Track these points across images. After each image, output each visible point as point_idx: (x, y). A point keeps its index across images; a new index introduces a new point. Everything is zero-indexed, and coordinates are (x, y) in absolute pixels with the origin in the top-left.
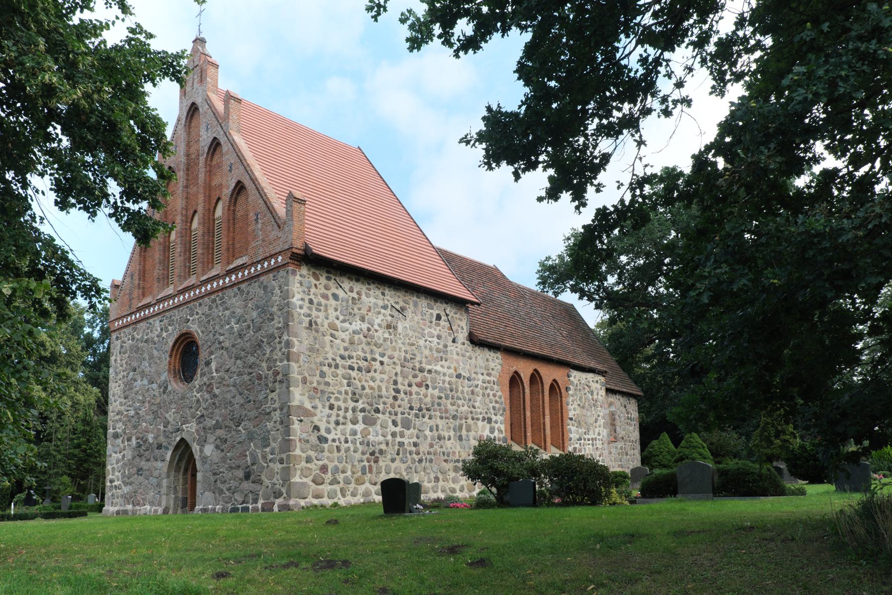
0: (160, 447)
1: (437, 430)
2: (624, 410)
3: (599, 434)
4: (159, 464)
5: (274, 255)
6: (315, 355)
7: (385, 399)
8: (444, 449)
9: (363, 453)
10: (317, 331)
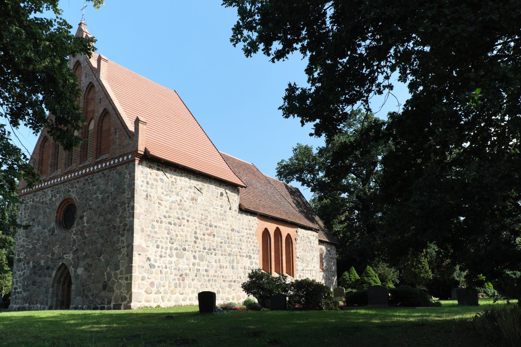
0: (48, 268)
4: (47, 279)
9: (176, 275)
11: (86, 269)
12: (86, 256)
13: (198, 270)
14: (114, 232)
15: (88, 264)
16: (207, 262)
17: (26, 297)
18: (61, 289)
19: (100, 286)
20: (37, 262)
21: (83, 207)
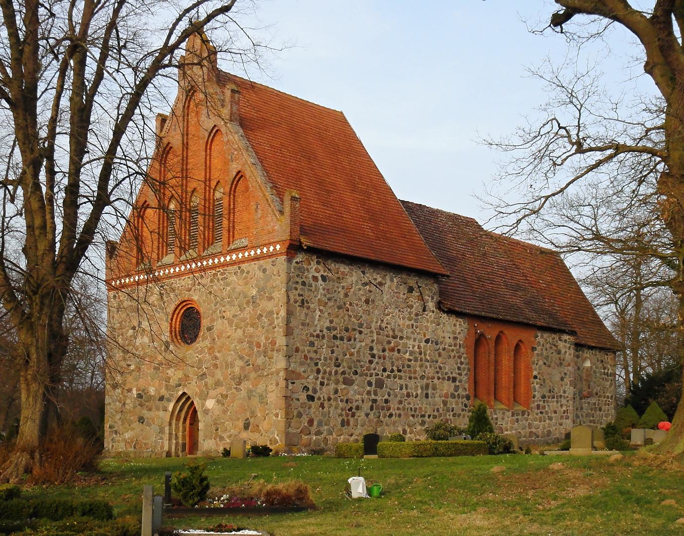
0: (161, 399)
1: (406, 388)
2: (601, 365)
3: (565, 392)
4: (161, 413)
5: (274, 244)
6: (306, 328)
7: (362, 363)
8: (412, 406)
9: (342, 410)
10: (308, 308)
11: (218, 402)
12: (218, 384)
13: (375, 401)
14: (258, 351)
15: (221, 395)
16: (388, 390)
17: (129, 438)
18: (181, 428)
19: (241, 424)
20: (143, 390)
21: (212, 315)
